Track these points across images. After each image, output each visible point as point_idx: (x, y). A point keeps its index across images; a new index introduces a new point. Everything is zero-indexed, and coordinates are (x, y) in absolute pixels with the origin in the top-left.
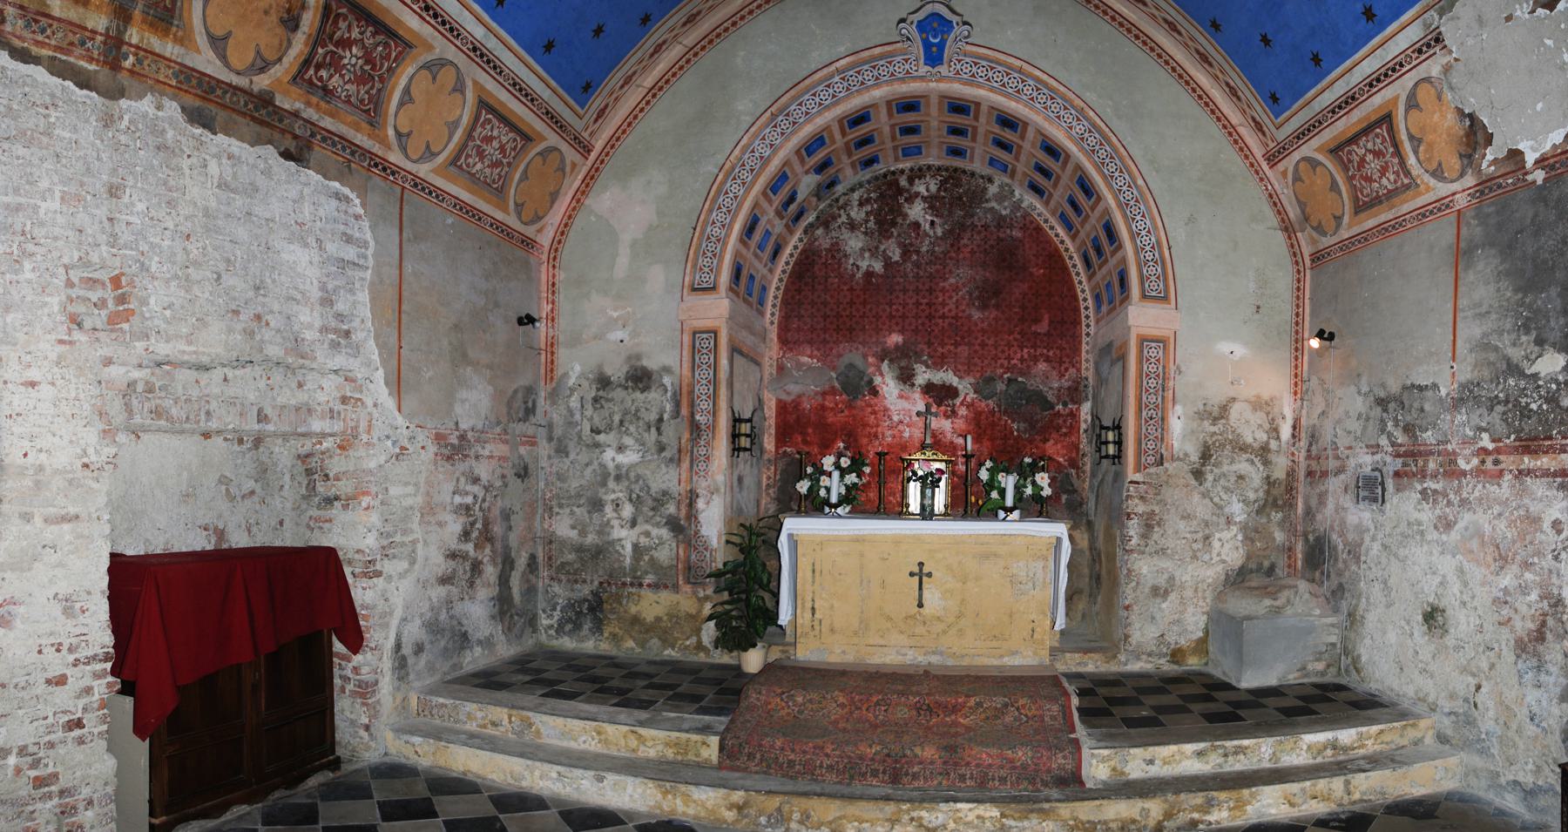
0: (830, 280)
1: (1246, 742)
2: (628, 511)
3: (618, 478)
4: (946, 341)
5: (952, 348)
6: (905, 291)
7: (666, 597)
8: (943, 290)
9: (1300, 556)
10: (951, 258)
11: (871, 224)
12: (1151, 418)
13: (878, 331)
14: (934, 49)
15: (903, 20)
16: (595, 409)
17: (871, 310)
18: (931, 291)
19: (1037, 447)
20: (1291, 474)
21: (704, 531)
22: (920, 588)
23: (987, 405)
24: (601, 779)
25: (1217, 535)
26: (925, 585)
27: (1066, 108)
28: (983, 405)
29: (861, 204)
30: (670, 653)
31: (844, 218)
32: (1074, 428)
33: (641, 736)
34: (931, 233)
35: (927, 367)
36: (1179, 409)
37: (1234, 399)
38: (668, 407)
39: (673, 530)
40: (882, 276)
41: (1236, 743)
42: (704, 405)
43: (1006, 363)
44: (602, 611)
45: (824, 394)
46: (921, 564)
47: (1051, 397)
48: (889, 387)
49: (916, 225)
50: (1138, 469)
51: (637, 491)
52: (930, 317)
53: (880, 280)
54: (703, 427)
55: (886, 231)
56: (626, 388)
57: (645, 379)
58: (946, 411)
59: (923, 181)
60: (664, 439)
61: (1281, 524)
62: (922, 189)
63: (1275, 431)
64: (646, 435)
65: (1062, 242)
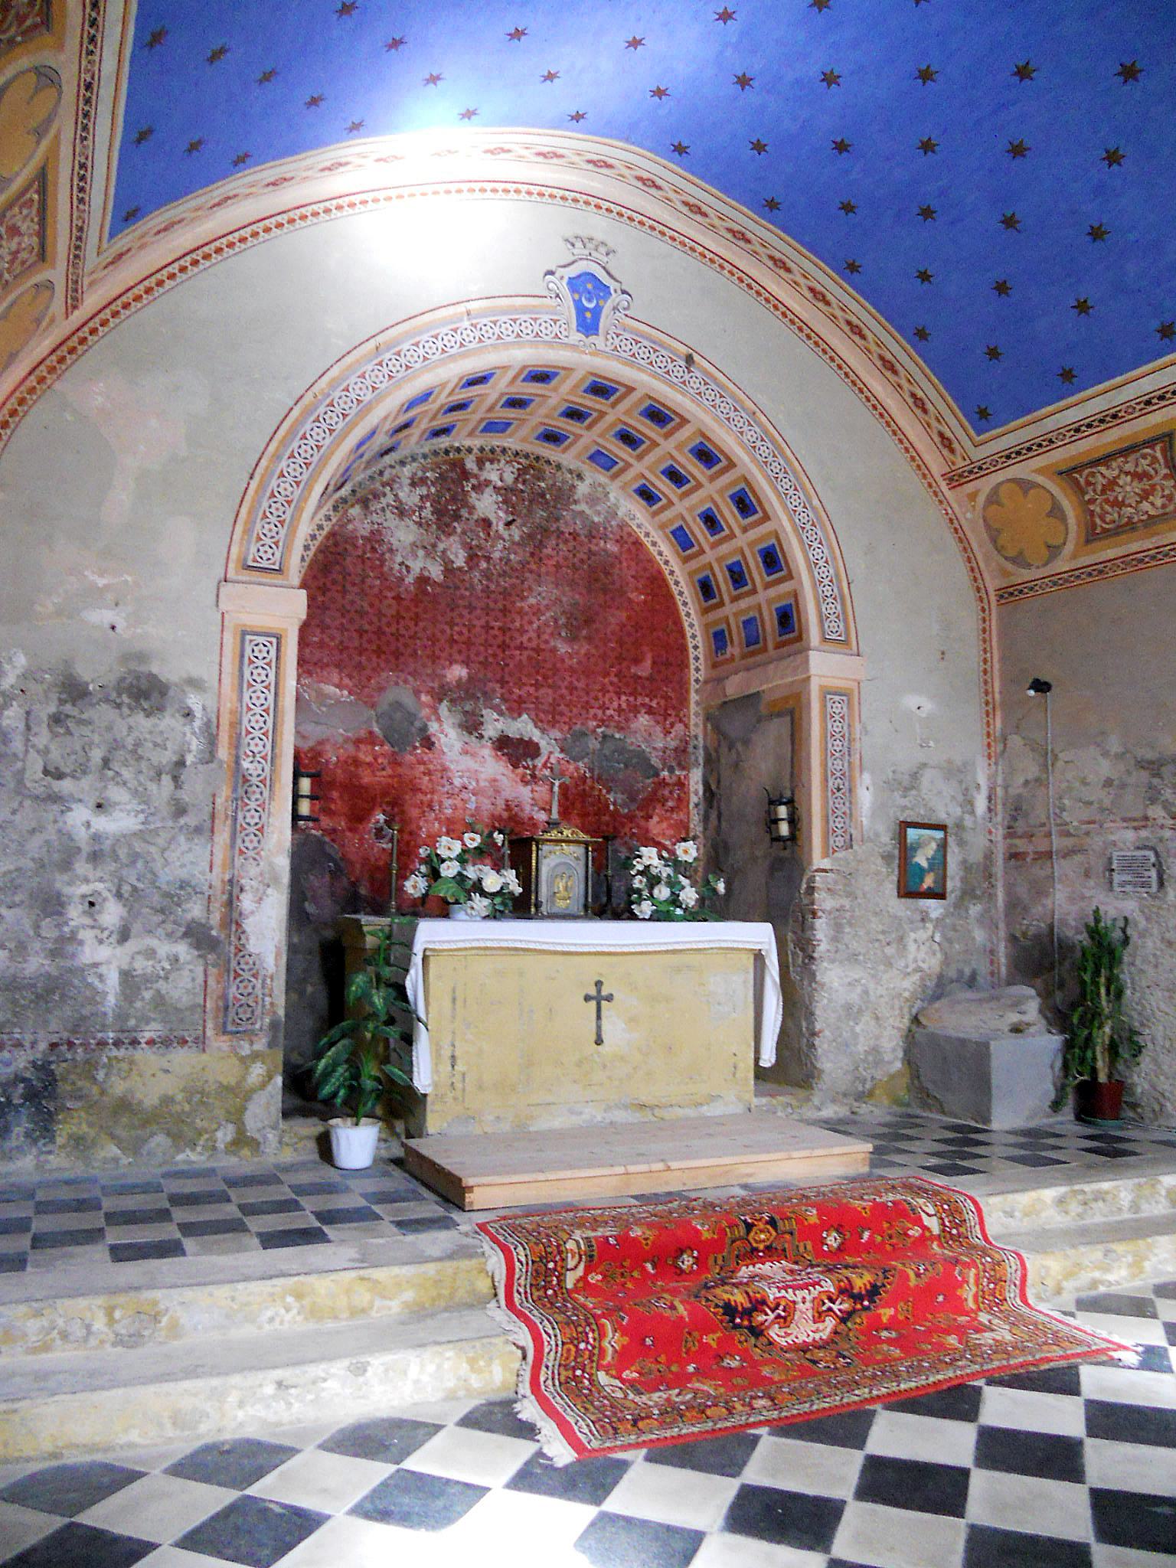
0: (368, 581)
1: (1106, 1186)
2: (112, 914)
3: (95, 857)
4: (524, 680)
5: (532, 690)
6: (471, 608)
7: (182, 1059)
8: (521, 612)
9: (1003, 960)
10: (531, 572)
11: (427, 513)
12: (839, 789)
13: (434, 658)
14: (588, 315)
15: (552, 273)
16: (55, 735)
17: (424, 629)
18: (505, 611)
19: (638, 827)
20: (989, 856)
21: (253, 946)
22: (599, 1017)
23: (577, 769)
24: (360, 1370)
25: (913, 935)
26: (604, 1013)
27: (736, 410)
28: (571, 768)
29: (413, 484)
30: (192, 1157)
31: (390, 499)
32: (682, 802)
33: (376, 1282)
34: (507, 537)
35: (501, 713)
36: (867, 778)
37: (924, 765)
38: (195, 744)
39: (197, 946)
40: (439, 585)
41: (1095, 1186)
42: (257, 745)
43: (600, 713)
44: (53, 1096)
45: (358, 742)
46: (599, 984)
47: (655, 761)
48: (448, 735)
49: (486, 523)
50: (825, 855)
51: (133, 880)
52: (503, 646)
53: (438, 590)
54: (254, 780)
55: (448, 525)
56: (118, 706)
57: (155, 695)
58: (524, 776)
59: (496, 466)
60: (185, 796)
61: (980, 921)
62: (494, 477)
63: (969, 804)
64: (152, 787)
65: (667, 562)
